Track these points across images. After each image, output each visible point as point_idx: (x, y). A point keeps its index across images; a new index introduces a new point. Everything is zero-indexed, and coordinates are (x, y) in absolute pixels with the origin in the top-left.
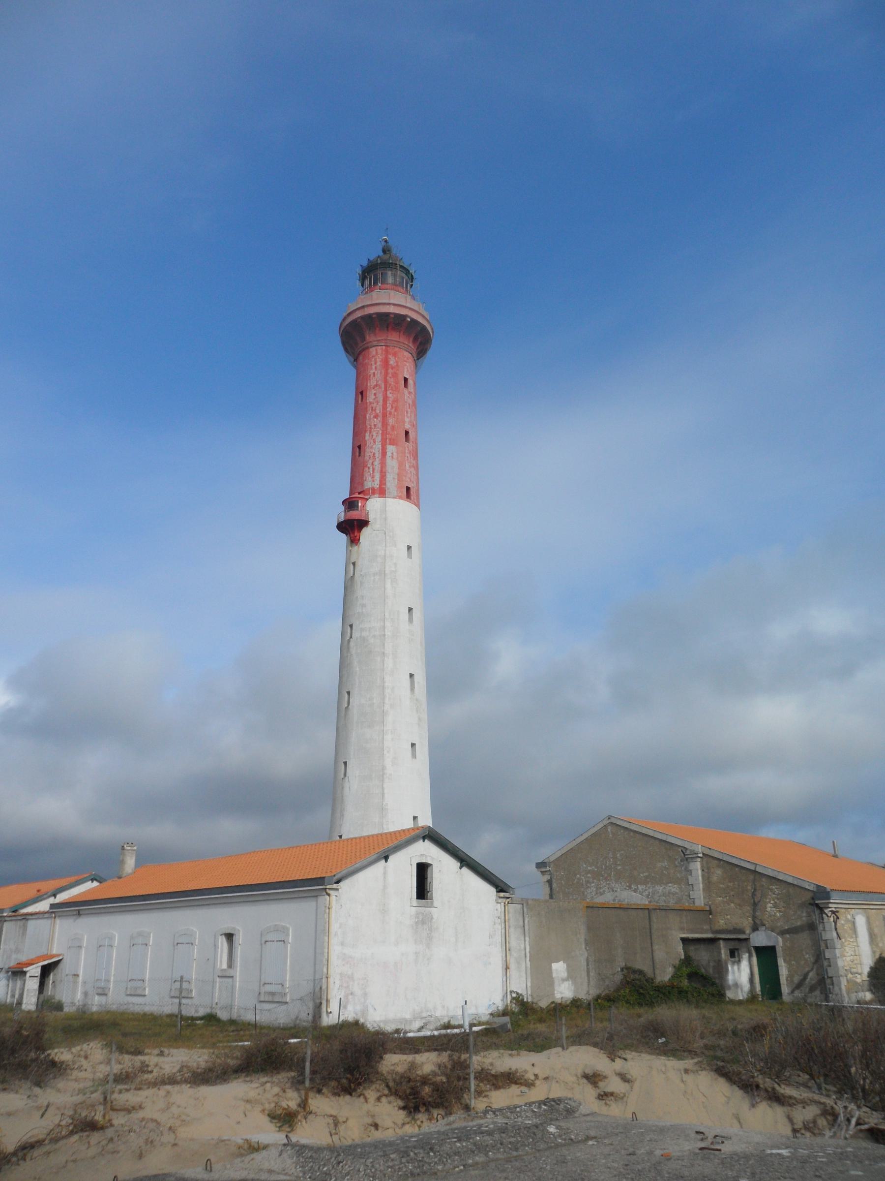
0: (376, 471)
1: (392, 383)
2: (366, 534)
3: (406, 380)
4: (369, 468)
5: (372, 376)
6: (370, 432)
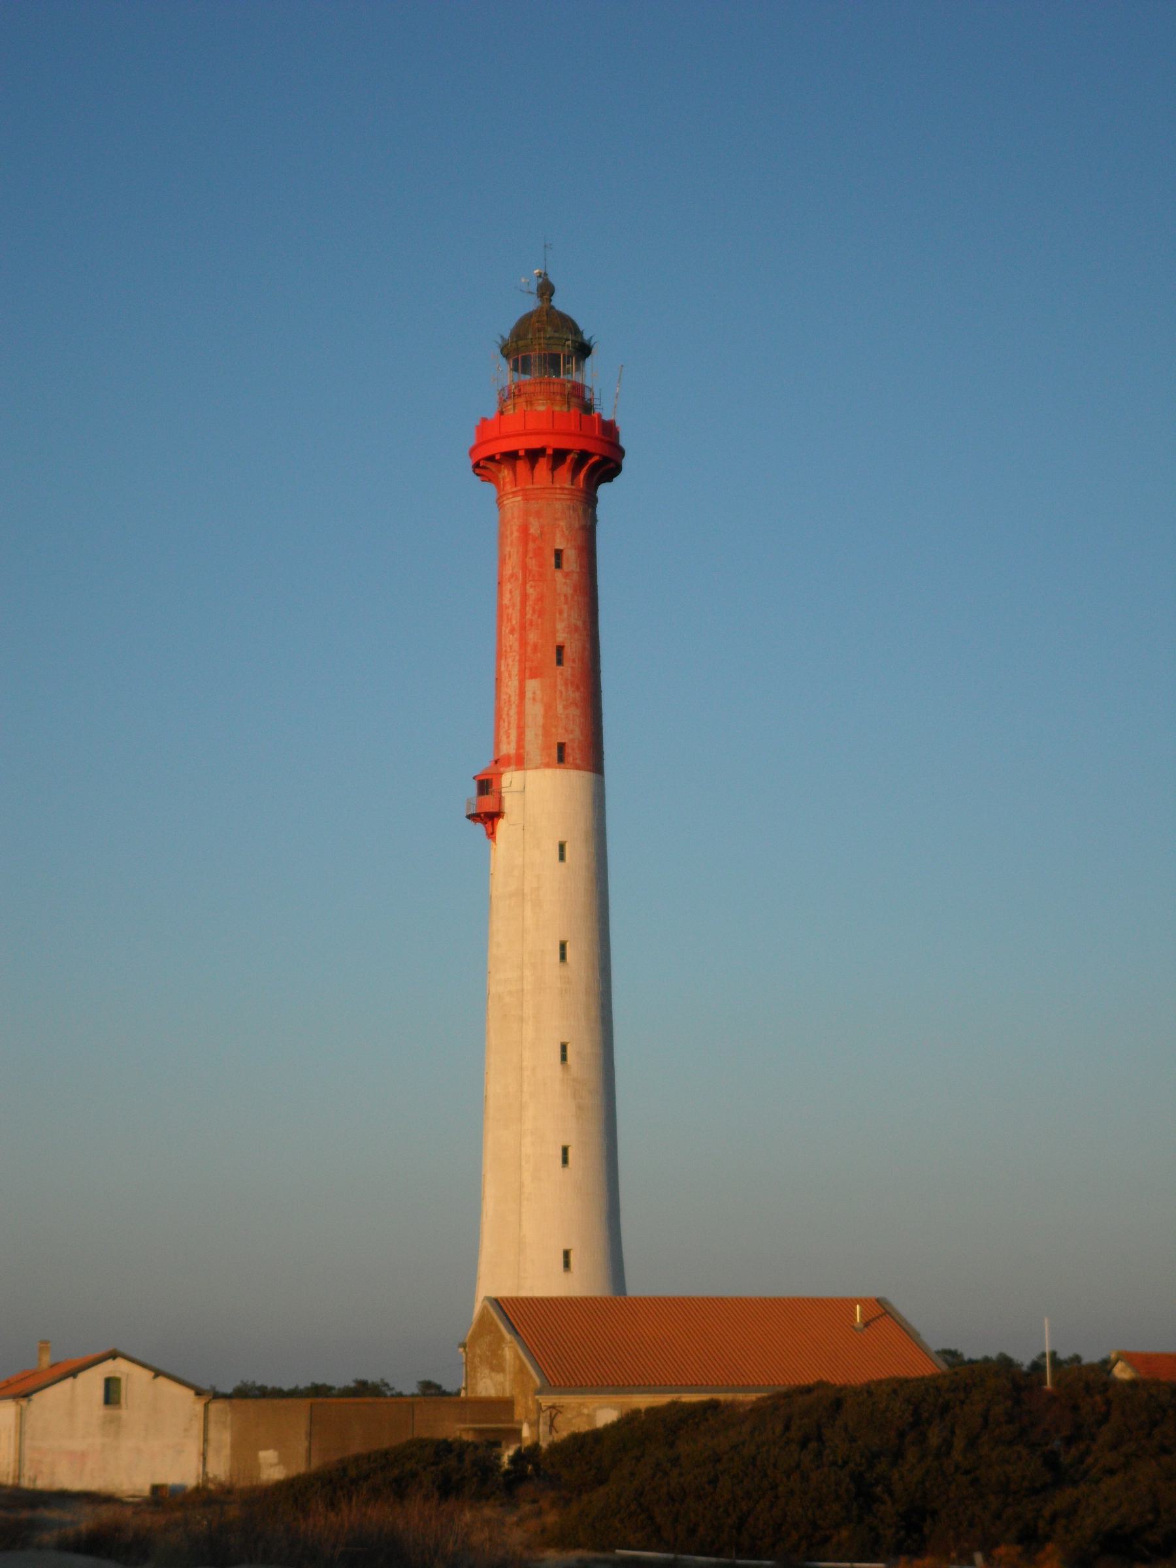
0: (512, 725)
1: (534, 568)
2: (502, 825)
3: (558, 554)
4: (504, 721)
5: (507, 558)
6: (506, 658)
